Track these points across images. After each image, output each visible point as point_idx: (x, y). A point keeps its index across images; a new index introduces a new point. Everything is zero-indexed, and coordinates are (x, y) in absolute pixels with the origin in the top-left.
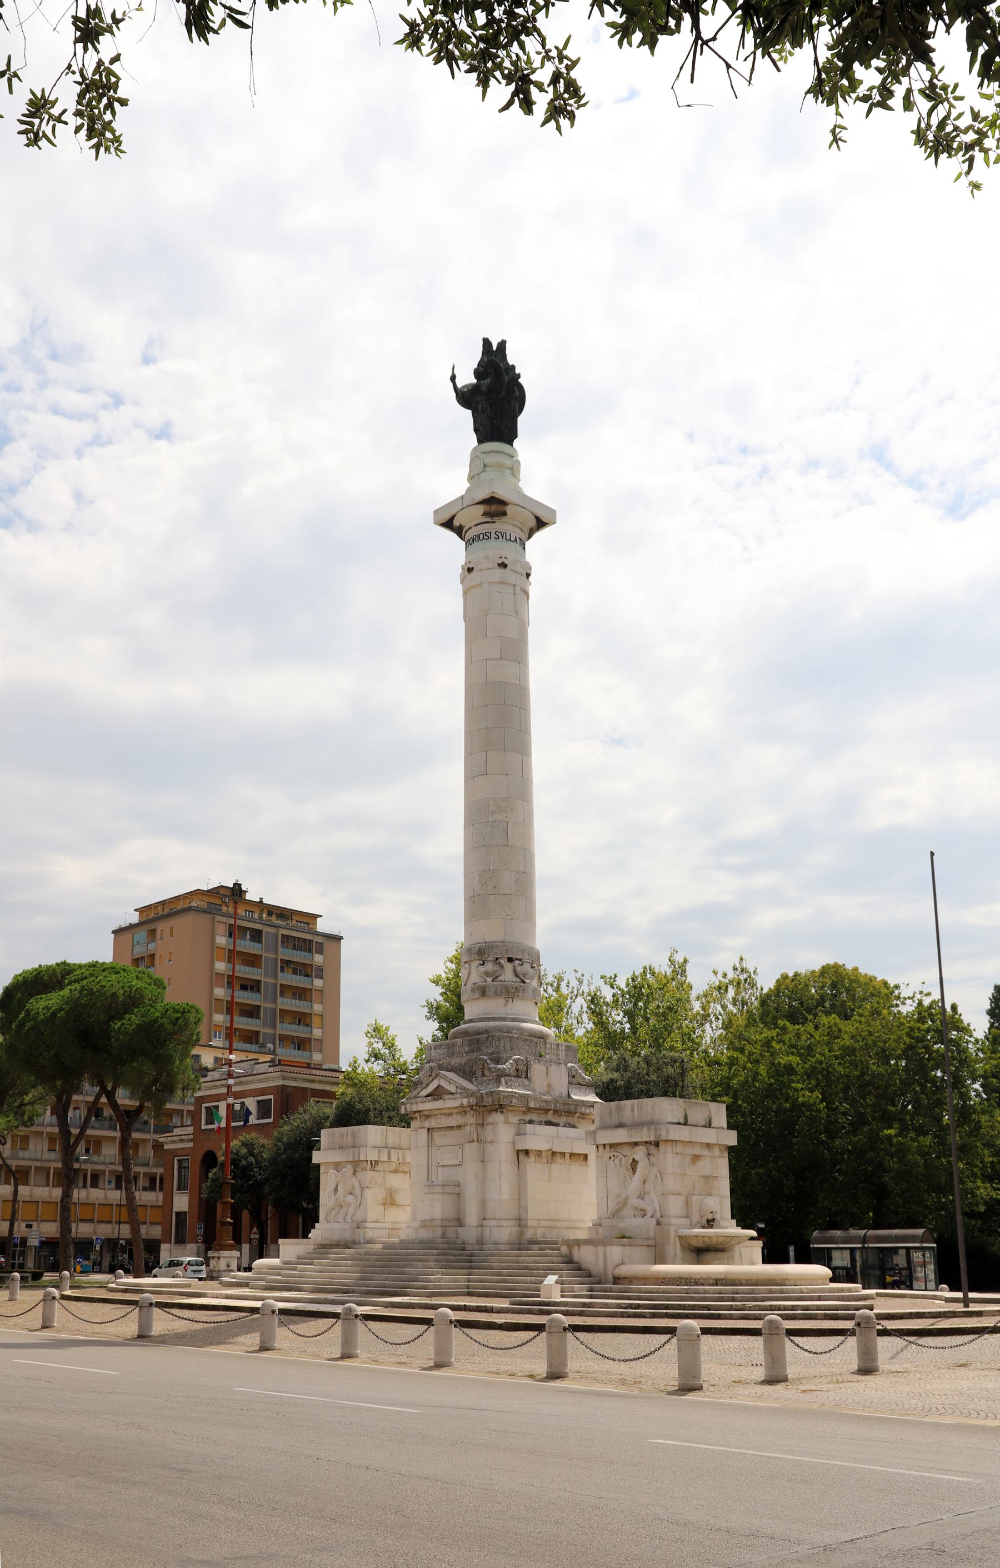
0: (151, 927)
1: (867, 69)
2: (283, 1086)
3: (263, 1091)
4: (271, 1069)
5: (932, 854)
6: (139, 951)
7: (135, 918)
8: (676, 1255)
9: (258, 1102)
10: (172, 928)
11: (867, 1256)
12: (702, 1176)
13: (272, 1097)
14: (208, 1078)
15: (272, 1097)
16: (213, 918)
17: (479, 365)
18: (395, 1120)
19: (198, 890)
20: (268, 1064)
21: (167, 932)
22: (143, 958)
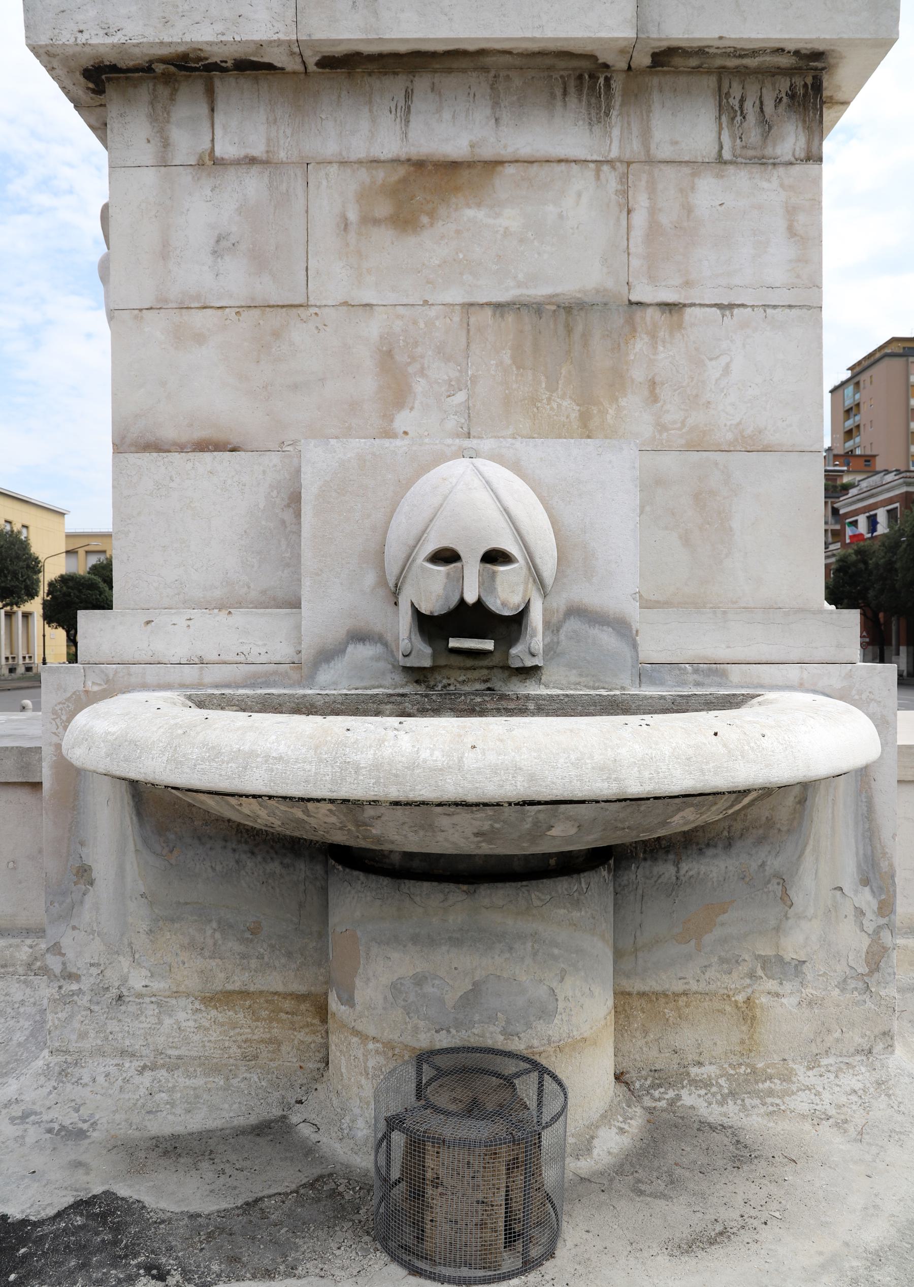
0: (856, 380)
1: (111, 609)
2: (907, 493)
3: (891, 501)
4: (897, 477)
5: (871, 444)
6: (848, 403)
7: (848, 374)
8: (84, 873)
9: (888, 511)
10: (871, 377)
11: (553, 304)
12: (499, 307)
13: (897, 505)
14: (850, 495)
15: (897, 505)
16: (907, 360)
17: (44, 609)
18: (54, 72)
19: (894, 340)
20: (895, 473)
21: (868, 381)
22: (851, 408)
